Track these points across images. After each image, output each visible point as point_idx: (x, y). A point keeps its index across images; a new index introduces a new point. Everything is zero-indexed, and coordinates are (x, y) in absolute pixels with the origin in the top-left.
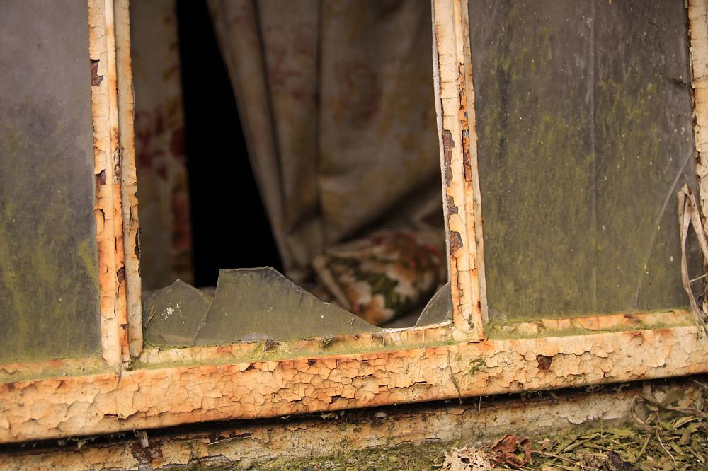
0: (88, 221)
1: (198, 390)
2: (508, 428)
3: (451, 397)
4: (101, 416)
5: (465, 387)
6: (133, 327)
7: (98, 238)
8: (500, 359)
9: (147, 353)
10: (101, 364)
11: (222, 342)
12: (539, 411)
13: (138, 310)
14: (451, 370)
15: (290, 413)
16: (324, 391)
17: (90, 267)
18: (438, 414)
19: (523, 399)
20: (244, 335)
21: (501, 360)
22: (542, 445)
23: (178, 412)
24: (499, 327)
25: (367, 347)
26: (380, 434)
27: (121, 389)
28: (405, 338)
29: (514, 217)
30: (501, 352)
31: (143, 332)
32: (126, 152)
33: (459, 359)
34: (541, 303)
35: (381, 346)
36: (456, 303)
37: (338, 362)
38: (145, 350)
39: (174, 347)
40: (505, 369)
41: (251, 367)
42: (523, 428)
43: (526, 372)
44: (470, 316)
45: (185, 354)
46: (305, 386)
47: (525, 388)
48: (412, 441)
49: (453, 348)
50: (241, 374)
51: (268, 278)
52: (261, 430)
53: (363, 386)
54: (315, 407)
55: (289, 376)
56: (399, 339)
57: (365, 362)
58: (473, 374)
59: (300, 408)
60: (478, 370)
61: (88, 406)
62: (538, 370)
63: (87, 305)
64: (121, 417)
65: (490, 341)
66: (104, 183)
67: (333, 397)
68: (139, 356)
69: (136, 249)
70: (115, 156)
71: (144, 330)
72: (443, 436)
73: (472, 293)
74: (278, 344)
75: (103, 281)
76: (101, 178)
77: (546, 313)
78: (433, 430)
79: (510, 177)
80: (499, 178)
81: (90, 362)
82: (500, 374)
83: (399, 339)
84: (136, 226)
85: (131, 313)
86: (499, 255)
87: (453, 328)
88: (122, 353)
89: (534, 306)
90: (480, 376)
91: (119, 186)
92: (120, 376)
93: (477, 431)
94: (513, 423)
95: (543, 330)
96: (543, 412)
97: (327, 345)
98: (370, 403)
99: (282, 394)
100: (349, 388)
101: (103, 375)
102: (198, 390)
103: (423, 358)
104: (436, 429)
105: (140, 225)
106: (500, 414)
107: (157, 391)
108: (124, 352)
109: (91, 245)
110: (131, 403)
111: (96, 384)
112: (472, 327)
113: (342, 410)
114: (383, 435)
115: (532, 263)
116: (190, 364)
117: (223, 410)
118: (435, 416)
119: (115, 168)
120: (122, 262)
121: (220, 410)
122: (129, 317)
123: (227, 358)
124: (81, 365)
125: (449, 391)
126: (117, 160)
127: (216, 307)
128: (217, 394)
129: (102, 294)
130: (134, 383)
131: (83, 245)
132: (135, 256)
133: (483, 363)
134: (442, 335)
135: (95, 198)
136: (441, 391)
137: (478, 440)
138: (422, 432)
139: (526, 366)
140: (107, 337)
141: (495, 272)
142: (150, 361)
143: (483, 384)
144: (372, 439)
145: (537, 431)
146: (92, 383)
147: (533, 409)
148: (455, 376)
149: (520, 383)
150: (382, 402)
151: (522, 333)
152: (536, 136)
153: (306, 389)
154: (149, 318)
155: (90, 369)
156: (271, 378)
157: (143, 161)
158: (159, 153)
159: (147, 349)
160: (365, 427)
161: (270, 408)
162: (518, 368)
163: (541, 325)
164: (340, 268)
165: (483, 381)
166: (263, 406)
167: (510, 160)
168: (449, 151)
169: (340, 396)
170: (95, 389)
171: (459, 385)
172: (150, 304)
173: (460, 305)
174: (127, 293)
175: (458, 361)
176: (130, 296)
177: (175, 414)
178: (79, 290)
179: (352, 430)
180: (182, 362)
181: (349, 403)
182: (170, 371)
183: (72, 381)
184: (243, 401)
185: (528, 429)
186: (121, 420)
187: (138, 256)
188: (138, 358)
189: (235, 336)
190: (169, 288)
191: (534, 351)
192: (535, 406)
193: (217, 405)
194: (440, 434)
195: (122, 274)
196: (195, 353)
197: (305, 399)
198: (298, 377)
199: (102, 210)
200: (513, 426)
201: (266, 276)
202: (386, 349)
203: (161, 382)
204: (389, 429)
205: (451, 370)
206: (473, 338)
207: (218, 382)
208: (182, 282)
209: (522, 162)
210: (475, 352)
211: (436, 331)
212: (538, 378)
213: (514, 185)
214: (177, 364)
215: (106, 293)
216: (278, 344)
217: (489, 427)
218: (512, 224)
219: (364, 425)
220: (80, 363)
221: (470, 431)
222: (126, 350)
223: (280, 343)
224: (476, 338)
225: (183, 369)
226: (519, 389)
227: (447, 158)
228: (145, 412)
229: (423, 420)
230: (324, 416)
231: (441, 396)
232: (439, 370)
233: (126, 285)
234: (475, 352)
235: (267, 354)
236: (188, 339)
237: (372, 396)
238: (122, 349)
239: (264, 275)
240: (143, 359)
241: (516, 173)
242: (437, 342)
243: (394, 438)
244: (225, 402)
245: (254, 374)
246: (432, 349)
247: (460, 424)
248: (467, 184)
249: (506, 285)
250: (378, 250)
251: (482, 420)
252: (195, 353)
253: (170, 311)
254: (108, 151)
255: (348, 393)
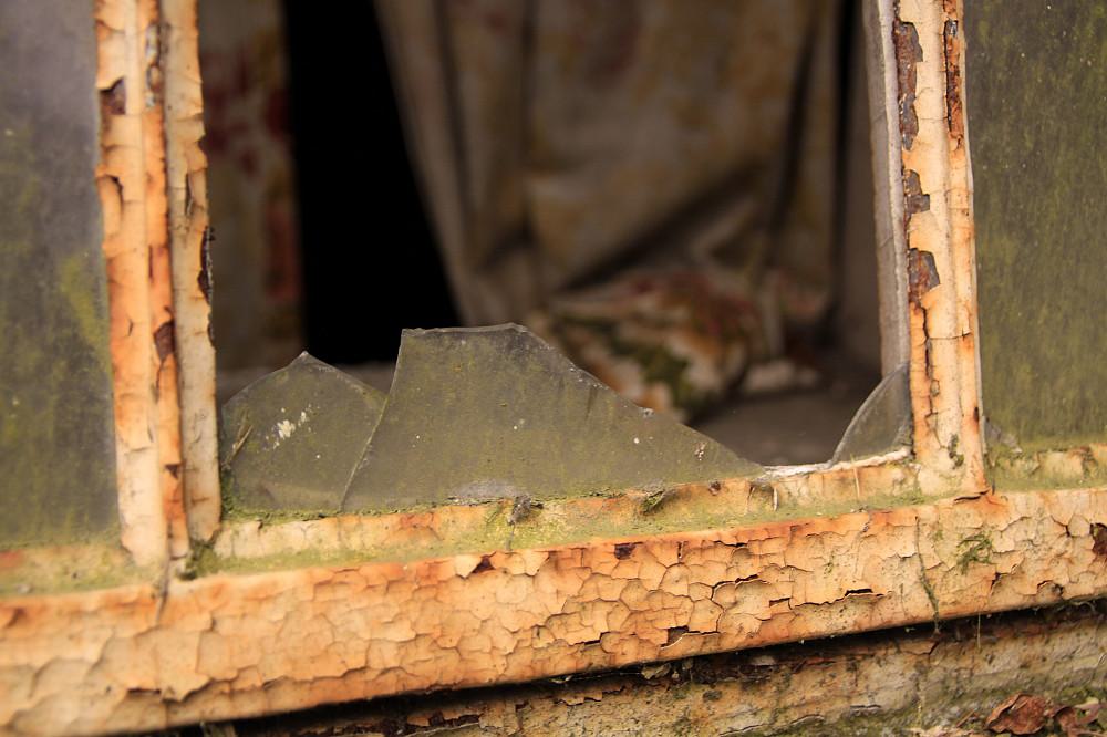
0: (83, 207)
1: (358, 622)
2: (1015, 677)
3: (918, 620)
4: (120, 695)
5: (949, 598)
6: (196, 470)
7: (108, 248)
8: (1019, 533)
9: (231, 532)
10: (118, 560)
11: (408, 501)
12: (1076, 639)
13: (209, 427)
14: (922, 561)
15: (573, 670)
16: (650, 616)
17: (87, 321)
18: (881, 653)
19: (1049, 618)
20: (459, 485)
21: (1021, 536)
22: (1084, 712)
23: (310, 678)
24: (1007, 463)
25: (739, 509)
26: (759, 702)
27: (168, 627)
28: (818, 488)
29: (1033, 224)
30: (1022, 519)
31: (221, 480)
32: (175, 35)
33: (938, 536)
34: (1083, 409)
35: (768, 507)
36: (920, 410)
37: (682, 547)
38: (227, 524)
39: (296, 516)
40: (1028, 555)
41: (484, 566)
42: (1041, 674)
43: (1070, 561)
44: (955, 440)
45: (323, 535)
46: (608, 608)
47: (1067, 596)
48: (822, 713)
49: (926, 511)
50: (460, 581)
51: (513, 351)
52: (500, 705)
53: (735, 604)
54: (629, 654)
55: (572, 584)
56: (804, 490)
57: (740, 548)
58: (963, 572)
59: (596, 659)
60: (975, 559)
61: (84, 670)
62: (1093, 556)
63: (82, 415)
64: (169, 696)
65: (999, 494)
66: (121, 110)
67: (670, 630)
68: (213, 541)
69: (202, 278)
70: (147, 44)
71: (224, 475)
72: (885, 700)
73: (960, 388)
74: (540, 506)
75: (120, 355)
76: (112, 98)
77: (1091, 431)
78: (867, 687)
79: (1026, 135)
80: (1006, 138)
81: (92, 557)
82: (1020, 567)
83: (804, 490)
84: (202, 220)
85: (190, 436)
86: (1002, 304)
87: (918, 466)
88: (170, 536)
89: (1069, 415)
90: (978, 571)
91: (158, 117)
92: (165, 595)
93: (953, 686)
94: (1024, 666)
95: (1093, 469)
96: (1084, 640)
97: (652, 509)
98: (750, 641)
99: (555, 627)
100: (706, 608)
101: (122, 590)
102: (358, 622)
103: (865, 535)
104: (873, 687)
105: (212, 219)
106: (1001, 651)
107: (259, 627)
108: (174, 532)
109: (90, 266)
110: (192, 660)
111: (107, 616)
112: (959, 463)
113: (688, 658)
114: (765, 703)
115: (1067, 322)
116: (335, 560)
117: (420, 669)
118: (874, 659)
119: (149, 73)
120: (167, 309)
121: (410, 670)
122: (187, 444)
123: (425, 542)
124: (68, 563)
125: (916, 607)
126: (152, 53)
127: (393, 420)
128: (403, 632)
129: (119, 389)
130: (201, 610)
131: (69, 267)
132: (200, 294)
133: (987, 543)
134: (895, 482)
135: (98, 151)
136: (899, 608)
137: (952, 703)
138: (845, 693)
139: (1070, 549)
140: (133, 493)
141: (995, 339)
142: (240, 553)
143: (984, 591)
144: (743, 713)
145: (1068, 679)
146: (95, 613)
147: (1066, 635)
148: (929, 575)
149: (1057, 586)
150: (776, 638)
151: (1051, 475)
152: (1078, 49)
153: (609, 614)
154: (235, 447)
155: (92, 574)
156: (532, 589)
157: (213, 142)
158: (241, 128)
159: (231, 522)
160: (727, 690)
161: (528, 663)
162: (1054, 552)
163: (1088, 457)
164: (578, 335)
165: (984, 583)
166: (511, 658)
167: (1026, 98)
168: (910, 71)
169: (685, 629)
170: (102, 627)
171: (936, 593)
172: (237, 412)
173: (932, 413)
174: (180, 386)
175: (935, 540)
176: (187, 394)
177: (303, 682)
178: (61, 378)
179: (700, 695)
180: (317, 553)
181: (704, 643)
182: (289, 578)
183: (43, 609)
184: (466, 646)
185: (1052, 676)
186: (169, 704)
187: (206, 296)
188: (210, 545)
189: (437, 489)
190: (283, 374)
191: (1085, 514)
192: (1070, 630)
193: (402, 659)
194: (882, 694)
195: (168, 338)
196: (348, 532)
197: (608, 637)
198: (591, 585)
199: (115, 180)
200: (1024, 671)
201: (510, 347)
202: (781, 516)
203: (266, 607)
204: (779, 691)
205: (922, 561)
206: (963, 486)
207: (407, 602)
208: (313, 360)
209: (1051, 103)
210: (970, 519)
211: (882, 470)
212: (1093, 573)
213: (1033, 153)
214: (305, 558)
215: (127, 385)
216: (540, 506)
217: (979, 677)
218: (1028, 237)
219: (727, 686)
220: (66, 558)
221: (939, 685)
222: (180, 528)
223: (545, 504)
224: (970, 486)
225: (321, 573)
226: (1055, 598)
227: (906, 86)
228: (230, 682)
229: (849, 670)
230: (648, 674)
231: (899, 619)
232: (897, 561)
233: (178, 367)
234: (970, 519)
235: (516, 532)
236: (327, 496)
237: (753, 625)
238: (170, 527)
239: (505, 344)
240: (222, 548)
241: (1039, 127)
242: (885, 496)
243: (786, 709)
244: (422, 652)
245: (490, 582)
246: (882, 515)
247: (922, 671)
248: (954, 144)
249: (1015, 371)
250: (648, 304)
251: (966, 662)
252: (348, 532)
253: (285, 429)
254: (131, 31)
255: (703, 620)
